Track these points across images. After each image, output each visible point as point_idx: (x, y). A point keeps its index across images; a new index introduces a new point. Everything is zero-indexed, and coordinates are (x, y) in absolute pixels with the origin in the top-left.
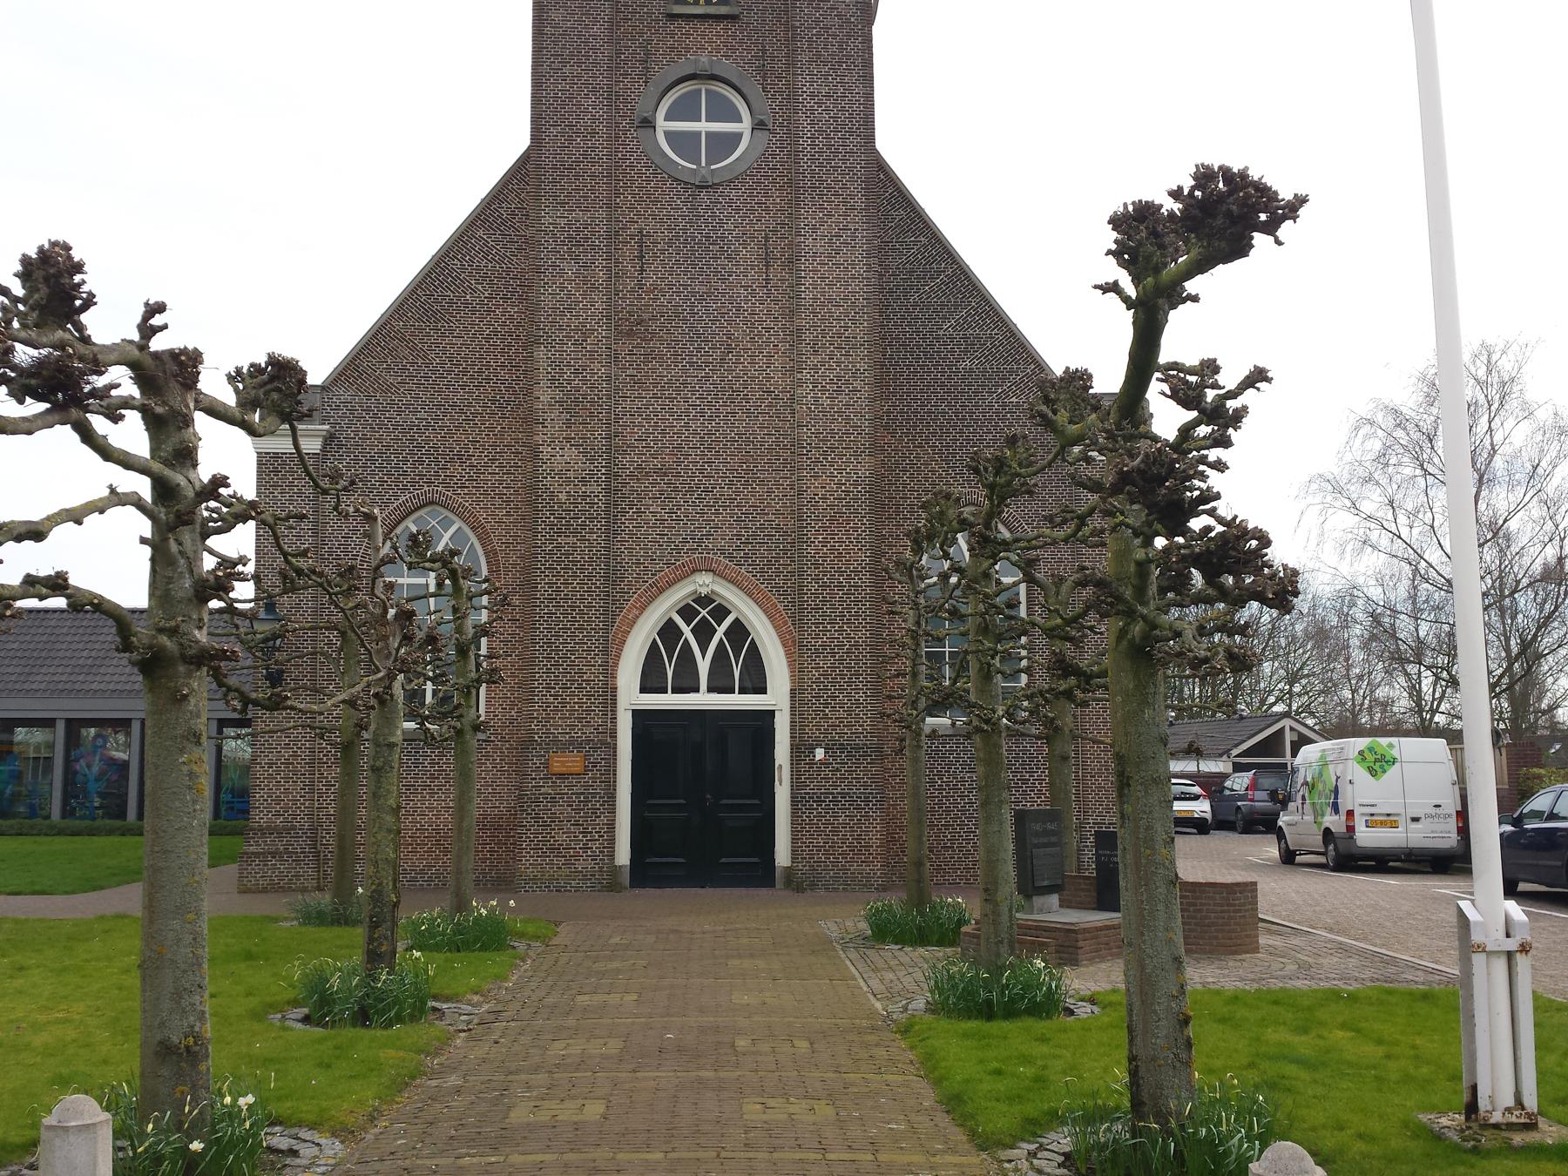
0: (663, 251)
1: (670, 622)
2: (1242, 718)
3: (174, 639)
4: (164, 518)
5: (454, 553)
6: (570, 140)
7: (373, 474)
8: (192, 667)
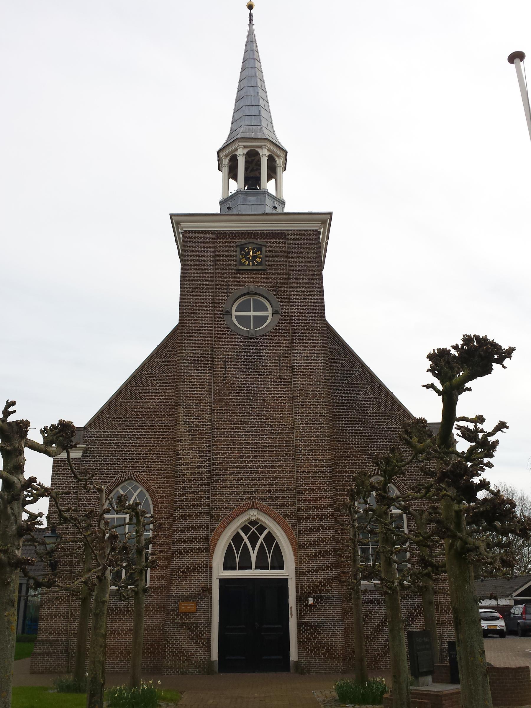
0: (234, 365)
1: (238, 534)
2: (516, 577)
3: (6, 555)
4: (6, 497)
5: (138, 504)
6: (195, 320)
7: (104, 466)
8: (13, 568)
